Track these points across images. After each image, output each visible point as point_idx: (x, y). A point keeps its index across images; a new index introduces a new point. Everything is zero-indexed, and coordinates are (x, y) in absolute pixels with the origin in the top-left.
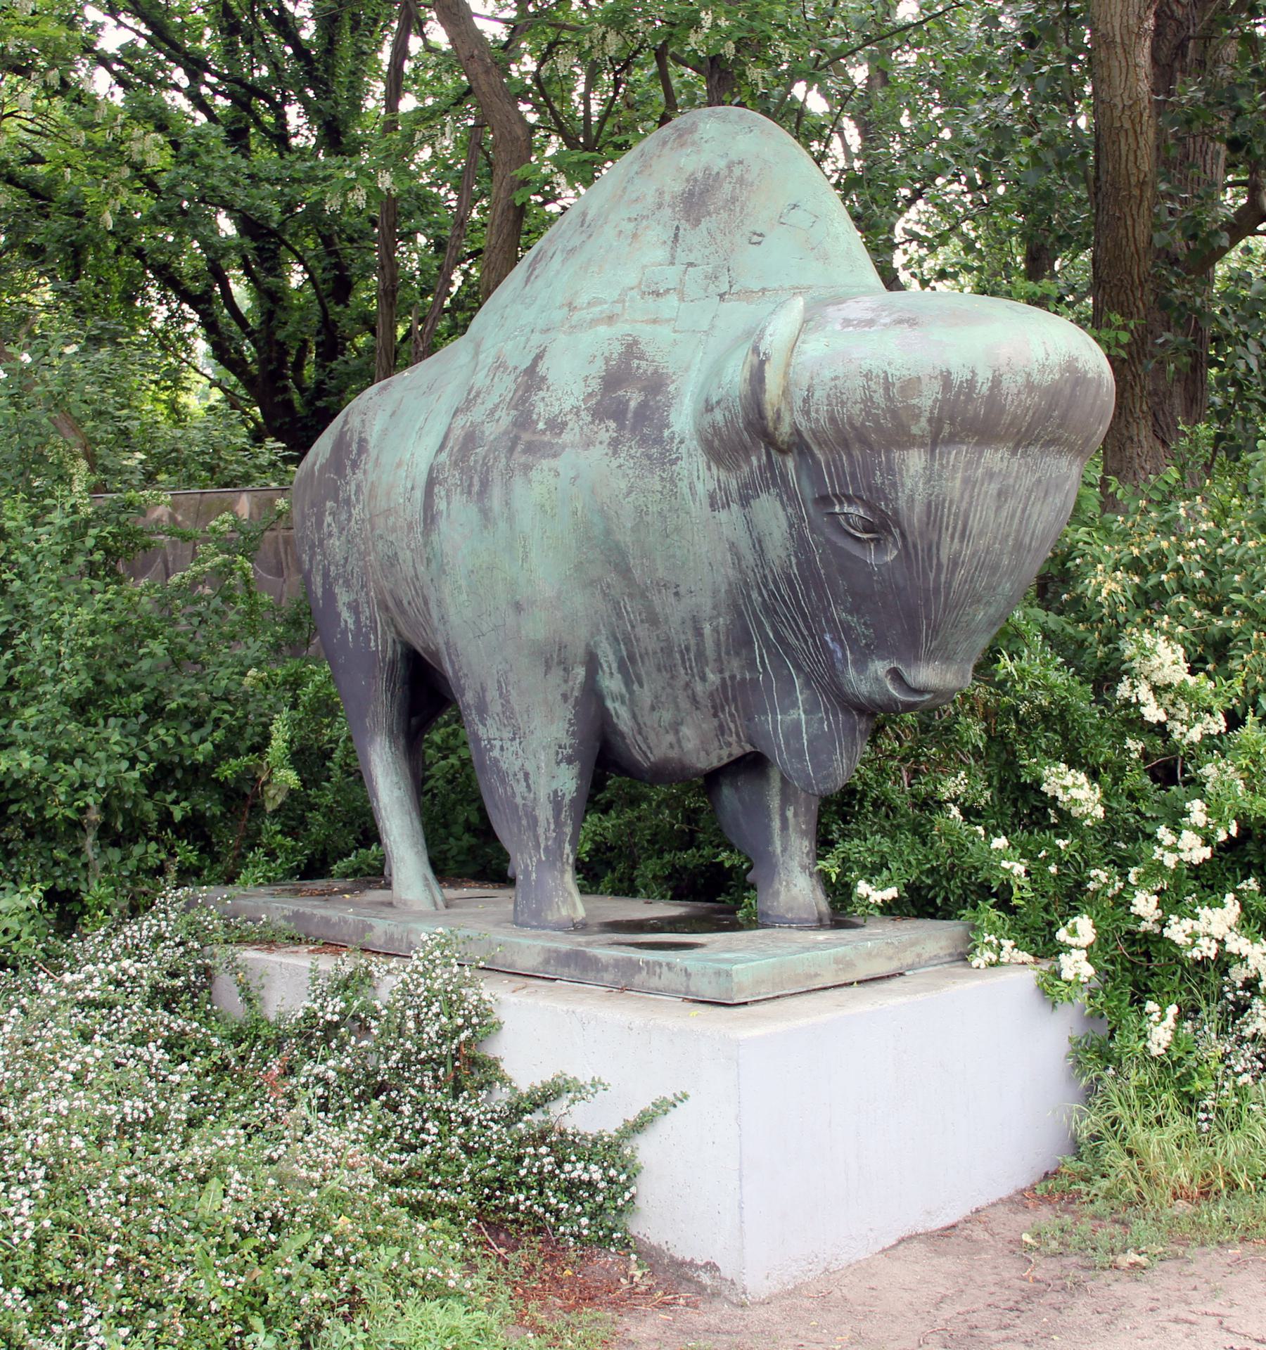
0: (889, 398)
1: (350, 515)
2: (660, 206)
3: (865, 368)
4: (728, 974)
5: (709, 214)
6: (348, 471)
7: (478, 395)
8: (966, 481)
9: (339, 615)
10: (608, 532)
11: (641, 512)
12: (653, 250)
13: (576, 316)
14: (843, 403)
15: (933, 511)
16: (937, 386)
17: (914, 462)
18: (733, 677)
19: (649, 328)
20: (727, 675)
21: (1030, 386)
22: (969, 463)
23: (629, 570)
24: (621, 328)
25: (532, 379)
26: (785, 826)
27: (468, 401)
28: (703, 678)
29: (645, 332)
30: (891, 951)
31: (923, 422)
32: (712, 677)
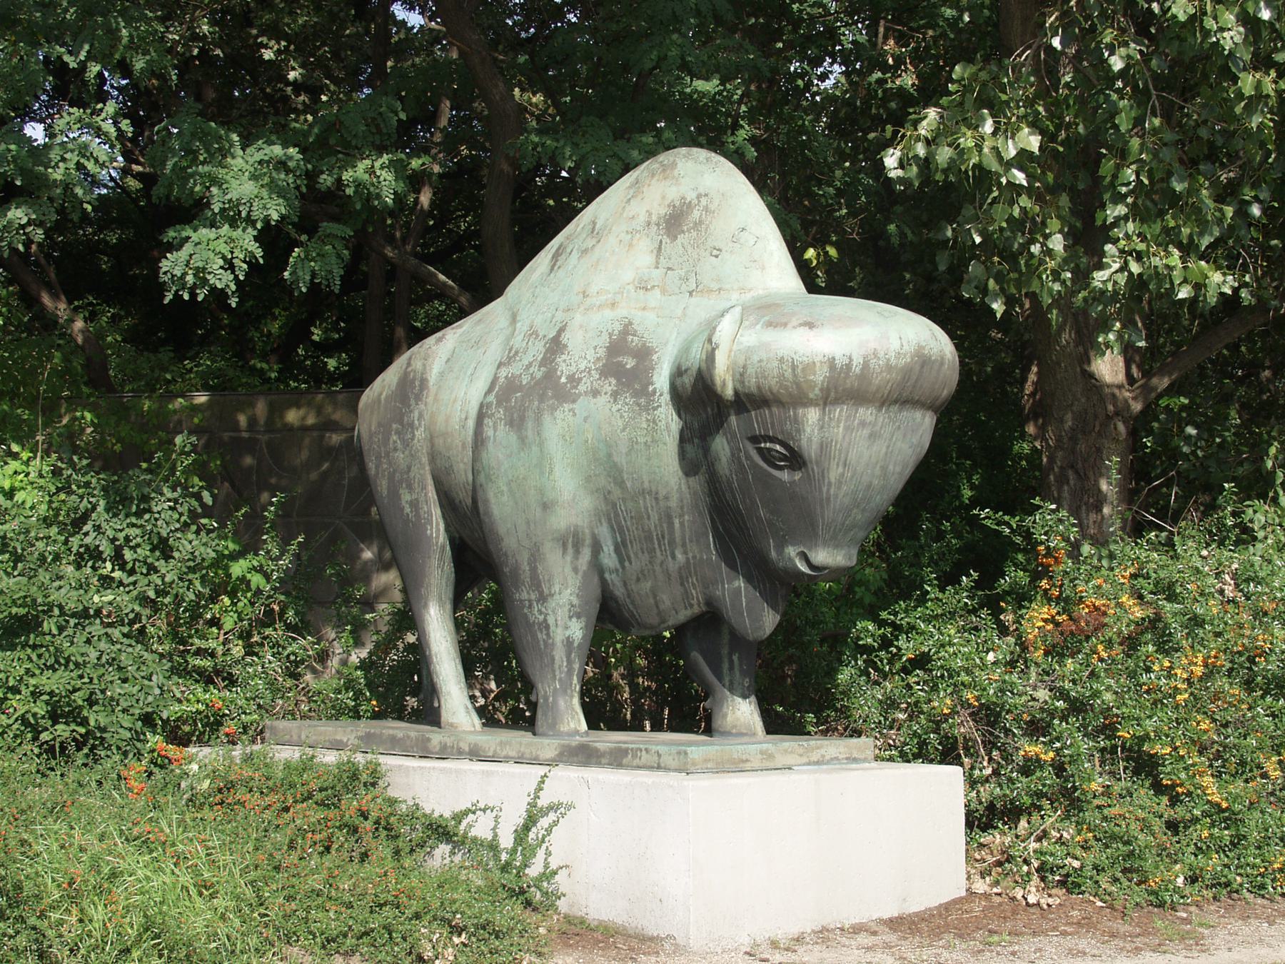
0: (795, 375)
1: (414, 435)
2: (649, 224)
3: (780, 355)
4: (686, 753)
5: (683, 232)
6: (412, 402)
7: (517, 353)
8: (847, 428)
9: (402, 509)
10: (610, 455)
11: (633, 443)
12: (642, 257)
13: (588, 301)
14: (766, 378)
15: (824, 446)
16: (826, 369)
17: (812, 415)
18: (694, 557)
19: (640, 313)
20: (690, 555)
21: (889, 367)
22: (848, 417)
23: (623, 482)
24: (622, 312)
25: (556, 346)
26: (731, 668)
27: (509, 358)
28: (674, 557)
29: (638, 317)
30: (801, 751)
31: (817, 391)
32: (680, 556)
